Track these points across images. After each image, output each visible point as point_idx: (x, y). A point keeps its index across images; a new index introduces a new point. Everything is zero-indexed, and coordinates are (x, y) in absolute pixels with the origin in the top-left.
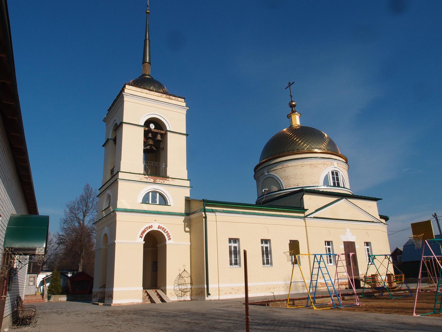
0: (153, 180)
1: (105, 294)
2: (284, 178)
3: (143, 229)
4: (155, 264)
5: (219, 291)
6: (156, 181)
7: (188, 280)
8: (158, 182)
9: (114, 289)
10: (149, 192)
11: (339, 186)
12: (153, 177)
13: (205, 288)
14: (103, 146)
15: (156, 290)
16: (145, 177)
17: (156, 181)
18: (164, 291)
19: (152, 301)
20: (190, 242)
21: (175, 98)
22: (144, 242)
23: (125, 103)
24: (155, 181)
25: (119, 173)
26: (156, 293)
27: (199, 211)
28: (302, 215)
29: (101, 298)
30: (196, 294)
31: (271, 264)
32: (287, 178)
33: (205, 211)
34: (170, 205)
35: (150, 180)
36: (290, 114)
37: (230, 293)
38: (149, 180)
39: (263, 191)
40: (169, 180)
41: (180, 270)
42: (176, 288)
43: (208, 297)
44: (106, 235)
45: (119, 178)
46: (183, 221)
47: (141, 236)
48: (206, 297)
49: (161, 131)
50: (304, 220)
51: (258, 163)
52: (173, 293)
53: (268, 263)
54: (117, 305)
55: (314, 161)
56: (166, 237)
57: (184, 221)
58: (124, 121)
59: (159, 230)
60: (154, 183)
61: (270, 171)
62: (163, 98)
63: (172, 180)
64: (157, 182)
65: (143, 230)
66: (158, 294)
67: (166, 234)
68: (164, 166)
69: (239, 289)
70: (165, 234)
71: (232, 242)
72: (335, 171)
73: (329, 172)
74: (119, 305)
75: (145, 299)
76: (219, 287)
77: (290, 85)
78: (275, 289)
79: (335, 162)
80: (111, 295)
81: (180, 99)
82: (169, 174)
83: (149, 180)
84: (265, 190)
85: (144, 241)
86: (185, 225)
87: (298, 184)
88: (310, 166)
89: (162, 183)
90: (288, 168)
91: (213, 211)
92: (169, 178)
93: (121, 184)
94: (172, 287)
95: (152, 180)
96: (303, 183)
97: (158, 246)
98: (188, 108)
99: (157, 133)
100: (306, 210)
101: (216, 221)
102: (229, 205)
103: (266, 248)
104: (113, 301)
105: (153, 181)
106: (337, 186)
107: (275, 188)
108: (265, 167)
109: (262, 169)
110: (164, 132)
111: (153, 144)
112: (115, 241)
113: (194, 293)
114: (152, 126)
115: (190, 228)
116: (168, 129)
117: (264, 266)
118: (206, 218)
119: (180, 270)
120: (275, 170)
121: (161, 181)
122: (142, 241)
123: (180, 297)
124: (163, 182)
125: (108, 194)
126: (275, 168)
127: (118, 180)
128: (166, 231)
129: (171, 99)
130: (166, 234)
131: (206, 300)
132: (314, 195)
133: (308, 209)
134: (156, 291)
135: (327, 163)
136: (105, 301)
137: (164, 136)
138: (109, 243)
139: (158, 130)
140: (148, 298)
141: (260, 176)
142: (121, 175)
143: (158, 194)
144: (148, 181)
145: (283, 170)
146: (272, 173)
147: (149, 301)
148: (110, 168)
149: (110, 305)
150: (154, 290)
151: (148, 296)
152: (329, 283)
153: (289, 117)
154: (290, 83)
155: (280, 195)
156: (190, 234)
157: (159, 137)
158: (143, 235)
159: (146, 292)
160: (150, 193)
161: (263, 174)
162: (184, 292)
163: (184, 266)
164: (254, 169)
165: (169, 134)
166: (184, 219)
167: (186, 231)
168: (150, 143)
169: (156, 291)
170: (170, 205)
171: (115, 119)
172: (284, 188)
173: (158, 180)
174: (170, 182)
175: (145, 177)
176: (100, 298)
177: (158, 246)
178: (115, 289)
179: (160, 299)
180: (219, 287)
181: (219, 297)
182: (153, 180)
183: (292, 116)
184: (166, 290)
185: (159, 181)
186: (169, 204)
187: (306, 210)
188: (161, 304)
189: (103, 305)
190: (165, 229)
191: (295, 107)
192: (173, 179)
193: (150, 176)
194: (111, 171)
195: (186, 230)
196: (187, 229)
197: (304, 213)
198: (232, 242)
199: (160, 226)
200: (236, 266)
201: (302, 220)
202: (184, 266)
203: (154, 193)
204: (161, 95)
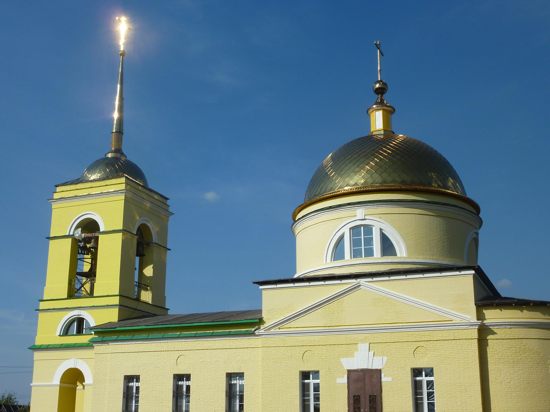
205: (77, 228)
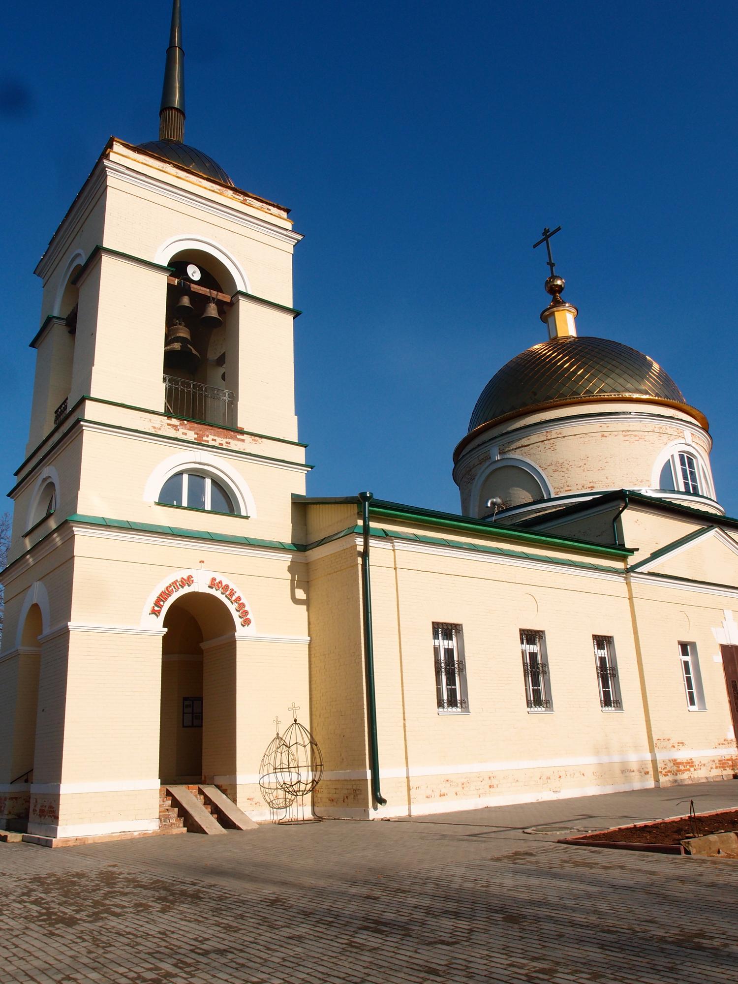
0: (196, 436)
1: (28, 801)
2: (553, 467)
3: (161, 588)
4: (187, 706)
5: (409, 789)
6: (205, 438)
7: (303, 755)
8: (211, 443)
9: (62, 786)
10: (180, 474)
11: (696, 494)
12: (196, 425)
13: (367, 780)
14: (33, 345)
15: (201, 786)
16: (169, 425)
17: (205, 438)
18: (230, 791)
19: (193, 827)
20: (309, 635)
21: (260, 204)
22: (166, 630)
23: (110, 194)
24: (200, 437)
25: (87, 401)
26: (202, 797)
27: (342, 534)
28: (620, 565)
29: (14, 816)
30: (332, 800)
31: (464, 703)
32: (559, 467)
33: (366, 533)
34: (247, 518)
35: (186, 434)
36: (549, 308)
37: (441, 796)
38: (183, 433)
39: (489, 505)
40: (243, 441)
41: (277, 722)
42: (266, 779)
43: (375, 808)
44: (35, 608)
45: (86, 418)
46: (289, 567)
47: (156, 608)
48: (371, 811)
49: (219, 293)
50: (626, 578)
51: (463, 433)
52: (258, 796)
53: (452, 702)
54: (71, 844)
55: (635, 424)
56: (235, 615)
57: (291, 569)
58: (105, 245)
59: (213, 592)
60: (199, 443)
61: (508, 451)
62: (228, 198)
64: (208, 442)
65: (163, 589)
66: (208, 801)
67: (236, 605)
68: (226, 398)
69: (465, 780)
70: (232, 608)
71: (440, 635)
72: (685, 455)
73: (672, 456)
74: (78, 843)
75: (167, 818)
76: (408, 778)
77: (547, 235)
78: (561, 780)
79: (688, 431)
80: (51, 807)
81: (274, 210)
82: (242, 422)
83: (183, 433)
84: (493, 503)
85: (164, 626)
86: (292, 581)
87: (591, 485)
88: (625, 436)
89: (224, 447)
90: (563, 439)
91: (386, 536)
92: (242, 432)
93: (91, 440)
94: (255, 778)
95: (191, 436)
96: (608, 481)
97: (204, 646)
98: (300, 237)
99: (206, 300)
100: (632, 551)
101: (395, 569)
103: (533, 656)
104: (59, 828)
105: (195, 439)
106: (692, 492)
107: (523, 496)
108: (495, 438)
109: (483, 447)
110: (227, 298)
111: (189, 337)
112: (69, 624)
113: (323, 794)
114: (194, 272)
115: (307, 592)
116: (240, 287)
117: (441, 710)
118: (365, 555)
119: (277, 722)
120: (523, 446)
122: (157, 627)
123: (279, 808)
124: (225, 444)
125: (44, 480)
126: (524, 442)
127: (82, 423)
128: (234, 598)
129: (250, 205)
130: (236, 605)
131: (371, 818)
132: (647, 512)
133: (637, 550)
134: (201, 792)
135: (669, 431)
136: (30, 827)
137: (229, 310)
138: (47, 631)
139: (210, 289)
140: (176, 815)
141: (474, 466)
142: (91, 411)
143: (208, 482)
144: (179, 435)
145: (548, 447)
146: (516, 455)
147: (182, 825)
148: (52, 405)
149: (48, 844)
150: (194, 788)
151: (176, 810)
152: (694, 760)
153: (547, 317)
154: (546, 231)
155: (541, 513)
156: (308, 610)
157: (212, 311)
158: (161, 607)
159: (169, 794)
160: (185, 477)
161: (488, 458)
162: (290, 790)
163: (294, 708)
164: (454, 455)
165: (244, 306)
166: (289, 564)
167: (296, 601)
168: (181, 335)
169: (201, 792)
170: (247, 518)
171: (75, 254)
172: (553, 496)
173: (211, 437)
174: (248, 445)
175: (169, 422)
176: (10, 817)
177: (204, 646)
178: (68, 788)
179: (216, 816)
180: (408, 778)
181: (410, 809)
182: (196, 436)
183: (556, 313)
184: (234, 786)
185: (211, 438)
186: (243, 513)
187: (632, 551)
188: (224, 835)
189: (23, 841)
190: (232, 590)
191: (561, 294)
192: (257, 438)
193: (186, 422)
194: (56, 412)
195: (297, 597)
196: (300, 594)
197: (623, 559)
198: (440, 635)
199: (217, 581)
200: (454, 709)
201: (620, 580)
202: (294, 708)
203: (198, 475)
204: (219, 190)
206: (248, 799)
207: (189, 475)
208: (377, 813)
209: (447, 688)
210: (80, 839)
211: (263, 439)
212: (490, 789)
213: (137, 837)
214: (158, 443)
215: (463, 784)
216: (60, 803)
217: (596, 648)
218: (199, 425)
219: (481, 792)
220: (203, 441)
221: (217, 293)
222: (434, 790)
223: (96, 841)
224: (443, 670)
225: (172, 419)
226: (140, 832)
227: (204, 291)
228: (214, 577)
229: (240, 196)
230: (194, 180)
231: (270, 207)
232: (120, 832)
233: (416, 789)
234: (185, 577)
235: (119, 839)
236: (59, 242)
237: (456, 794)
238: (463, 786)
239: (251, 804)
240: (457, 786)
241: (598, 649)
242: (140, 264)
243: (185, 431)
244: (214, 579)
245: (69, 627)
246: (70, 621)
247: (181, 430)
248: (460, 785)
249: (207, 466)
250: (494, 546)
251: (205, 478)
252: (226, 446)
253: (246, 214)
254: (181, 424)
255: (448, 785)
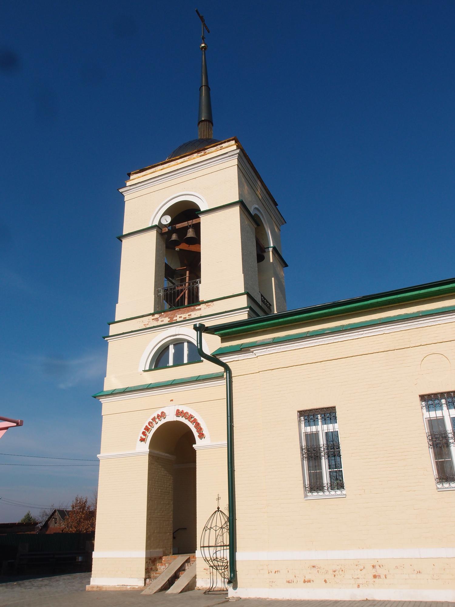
0: (169, 319)
3: (196, 416)
8: (179, 320)
16: (153, 319)
17: (174, 319)
21: (188, 157)
24: (171, 318)
37: (305, 582)
40: (200, 309)
63: (207, 306)
74: (98, 589)
89: (187, 319)
95: (166, 320)
102: (234, 329)
105: (169, 321)
112: (194, 446)
121: (184, 316)
122: (145, 448)
143: (186, 344)
144: (159, 323)
160: (171, 348)
173: (178, 316)
182: (169, 319)
193: (163, 313)
205: (165, 214)
206: (205, 569)
207: (173, 345)
208: (236, 593)
209: (436, 462)
210: (99, 587)
211: (214, 302)
212: (375, 580)
213: (129, 590)
214: (185, 325)
215: (334, 571)
216: (93, 563)
217: (303, 425)
218: (171, 312)
219: (360, 581)
220: (173, 321)
221: (188, 222)
222: (296, 575)
223: (108, 590)
224: (323, 454)
225: (155, 315)
226: (131, 586)
227: (182, 225)
228: (177, 409)
229: (202, 153)
230: (174, 163)
231: (222, 145)
232: (122, 585)
233: (275, 573)
234: (185, 412)
235: (119, 590)
236: (272, 206)
237: (325, 581)
238: (334, 573)
239: (207, 573)
240: (327, 572)
241: (323, 424)
242: (140, 233)
243: (162, 319)
244: (178, 410)
245: (194, 448)
246: (195, 443)
247: (160, 320)
248: (331, 572)
249: (178, 336)
250: (377, 318)
251: (184, 343)
252: (188, 318)
253: (198, 162)
254: (160, 316)
255: (315, 571)
